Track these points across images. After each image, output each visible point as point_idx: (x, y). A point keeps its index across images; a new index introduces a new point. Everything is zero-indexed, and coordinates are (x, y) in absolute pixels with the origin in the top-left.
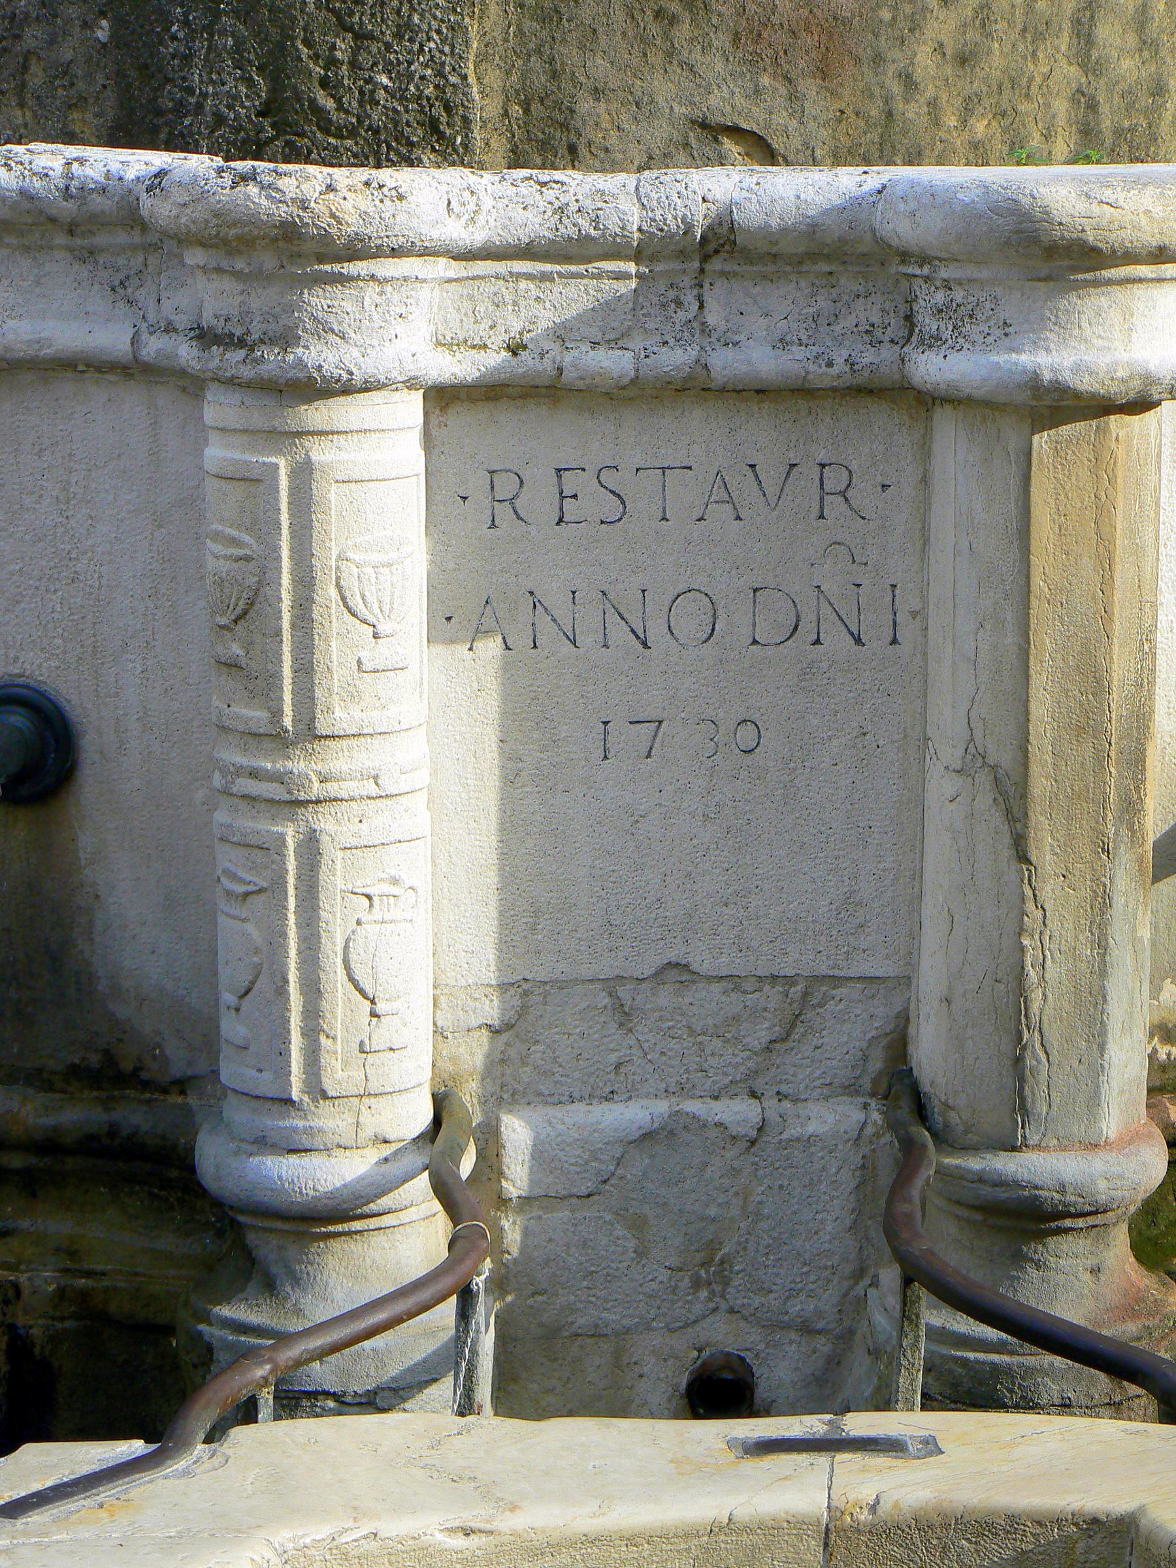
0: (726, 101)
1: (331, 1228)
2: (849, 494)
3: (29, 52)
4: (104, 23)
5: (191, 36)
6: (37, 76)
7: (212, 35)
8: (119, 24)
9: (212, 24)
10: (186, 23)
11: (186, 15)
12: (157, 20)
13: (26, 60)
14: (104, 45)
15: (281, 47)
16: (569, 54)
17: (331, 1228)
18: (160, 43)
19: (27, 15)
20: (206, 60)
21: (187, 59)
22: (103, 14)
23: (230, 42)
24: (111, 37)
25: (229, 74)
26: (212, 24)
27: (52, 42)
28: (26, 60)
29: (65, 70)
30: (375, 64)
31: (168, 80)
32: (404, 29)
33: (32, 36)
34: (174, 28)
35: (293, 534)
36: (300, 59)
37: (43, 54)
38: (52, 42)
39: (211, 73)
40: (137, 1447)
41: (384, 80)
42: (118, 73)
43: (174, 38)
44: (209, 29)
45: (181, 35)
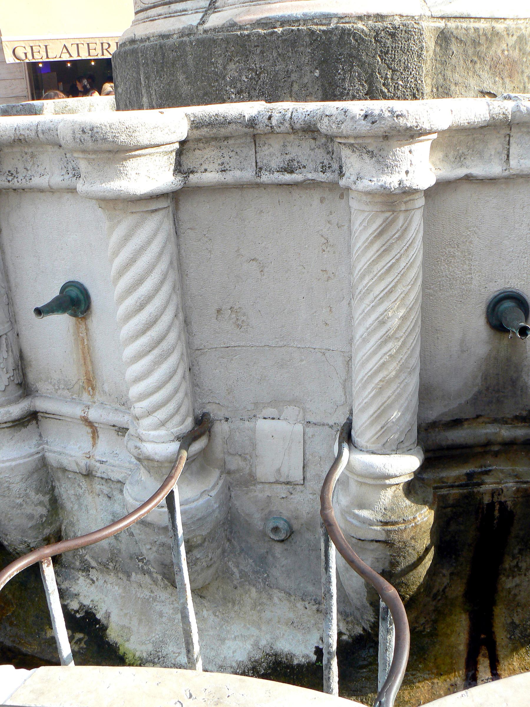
0: (488, 86)
4: (317, 71)
5: (345, 73)
6: (296, 87)
7: (351, 73)
8: (322, 71)
10: (343, 69)
11: (343, 67)
13: (292, 83)
15: (372, 74)
16: (449, 73)
19: (292, 70)
21: (344, 80)
22: (317, 68)
23: (357, 74)
27: (301, 77)
28: (292, 83)
32: (406, 68)
33: (294, 77)
34: (339, 71)
37: (298, 81)
38: (301, 77)
41: (401, 83)
43: (339, 74)
45: (342, 73)
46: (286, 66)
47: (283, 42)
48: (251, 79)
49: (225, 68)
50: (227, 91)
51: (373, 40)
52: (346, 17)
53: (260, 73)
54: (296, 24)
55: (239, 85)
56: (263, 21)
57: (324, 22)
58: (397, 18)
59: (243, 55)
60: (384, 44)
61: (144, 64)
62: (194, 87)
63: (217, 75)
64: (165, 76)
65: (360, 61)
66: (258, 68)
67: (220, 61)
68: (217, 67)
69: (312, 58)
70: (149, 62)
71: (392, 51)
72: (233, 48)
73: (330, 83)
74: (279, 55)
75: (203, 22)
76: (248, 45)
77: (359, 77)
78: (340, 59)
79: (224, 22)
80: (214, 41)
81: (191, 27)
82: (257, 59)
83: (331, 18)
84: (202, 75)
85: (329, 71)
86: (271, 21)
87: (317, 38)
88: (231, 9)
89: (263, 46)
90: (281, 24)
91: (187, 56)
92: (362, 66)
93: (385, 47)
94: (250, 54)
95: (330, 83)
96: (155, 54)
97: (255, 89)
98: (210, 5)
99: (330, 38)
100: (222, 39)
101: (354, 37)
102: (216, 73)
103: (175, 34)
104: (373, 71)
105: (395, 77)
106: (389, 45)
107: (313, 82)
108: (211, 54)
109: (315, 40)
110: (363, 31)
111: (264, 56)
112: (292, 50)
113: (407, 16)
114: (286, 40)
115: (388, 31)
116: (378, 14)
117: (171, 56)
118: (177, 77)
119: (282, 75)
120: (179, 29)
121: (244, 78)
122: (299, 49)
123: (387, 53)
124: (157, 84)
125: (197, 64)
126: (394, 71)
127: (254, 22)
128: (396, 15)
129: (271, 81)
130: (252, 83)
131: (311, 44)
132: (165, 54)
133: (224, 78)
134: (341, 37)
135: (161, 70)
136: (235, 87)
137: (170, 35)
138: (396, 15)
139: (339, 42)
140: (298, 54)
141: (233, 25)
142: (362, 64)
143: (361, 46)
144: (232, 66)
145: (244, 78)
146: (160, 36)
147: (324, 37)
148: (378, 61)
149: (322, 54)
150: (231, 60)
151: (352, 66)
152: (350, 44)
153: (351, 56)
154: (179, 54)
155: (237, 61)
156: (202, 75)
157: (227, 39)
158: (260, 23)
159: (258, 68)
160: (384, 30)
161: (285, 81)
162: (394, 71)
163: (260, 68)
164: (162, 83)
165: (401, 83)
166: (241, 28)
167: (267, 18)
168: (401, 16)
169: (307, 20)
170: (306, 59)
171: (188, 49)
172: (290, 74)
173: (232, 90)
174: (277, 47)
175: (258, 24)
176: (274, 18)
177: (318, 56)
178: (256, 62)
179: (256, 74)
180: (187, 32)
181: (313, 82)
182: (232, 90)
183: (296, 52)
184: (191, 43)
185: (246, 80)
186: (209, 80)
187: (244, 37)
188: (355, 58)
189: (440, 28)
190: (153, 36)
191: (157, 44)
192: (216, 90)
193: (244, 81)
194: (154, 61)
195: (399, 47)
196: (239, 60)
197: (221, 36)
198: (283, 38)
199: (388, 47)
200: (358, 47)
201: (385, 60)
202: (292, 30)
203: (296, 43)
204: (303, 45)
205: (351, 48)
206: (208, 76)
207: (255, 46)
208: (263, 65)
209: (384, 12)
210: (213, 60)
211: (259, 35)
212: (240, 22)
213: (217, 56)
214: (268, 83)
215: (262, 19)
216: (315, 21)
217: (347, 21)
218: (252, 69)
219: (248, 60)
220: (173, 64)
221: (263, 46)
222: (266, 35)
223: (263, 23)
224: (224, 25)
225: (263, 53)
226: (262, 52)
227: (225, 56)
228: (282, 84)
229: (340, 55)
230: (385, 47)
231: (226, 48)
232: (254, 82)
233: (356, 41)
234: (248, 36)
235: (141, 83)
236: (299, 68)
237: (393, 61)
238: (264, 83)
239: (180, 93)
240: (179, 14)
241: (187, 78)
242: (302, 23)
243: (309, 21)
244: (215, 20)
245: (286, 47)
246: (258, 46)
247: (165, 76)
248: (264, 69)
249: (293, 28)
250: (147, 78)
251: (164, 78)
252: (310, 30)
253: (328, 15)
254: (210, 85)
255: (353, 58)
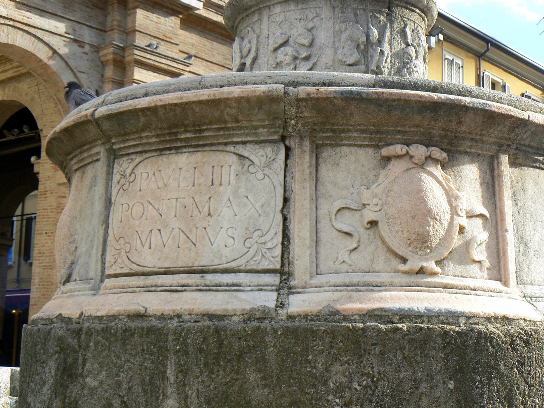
1: (415, 9)
2: (131, 184)
3: (422, 393)
4: (452, 382)
5: (483, 387)
7: (489, 386)
8: (457, 382)
9: (489, 382)
10: (481, 382)
11: (481, 378)
12: (470, 381)
13: (420, 396)
14: (452, 390)
15: (511, 390)
17: (415, 9)
18: (472, 390)
19: (421, 379)
20: (488, 395)
21: (482, 395)
22: (451, 379)
23: (496, 389)
24: (454, 387)
25: (496, 400)
26: (489, 382)
27: (432, 389)
28: (420, 396)
29: (437, 400)
30: (535, 396)
31: (475, 403)
33: (423, 388)
34: (477, 384)
35: (401, 88)
36: (517, 394)
37: (428, 394)
38: (432, 389)
39: (490, 400)
40: (21, 206)
41: (537, 401)
42: (457, 401)
43: (477, 387)
44: (488, 384)
45: (480, 386)
46: (414, 373)
47: (410, 342)
48: (365, 387)
49: (327, 370)
50: (328, 401)
51: (510, 347)
52: (474, 316)
53: (378, 380)
54: (419, 321)
55: (347, 395)
56: (376, 313)
57: (451, 320)
58: (522, 322)
59: (355, 354)
60: (521, 353)
61: (178, 351)
62: (275, 391)
63: (315, 378)
64: (221, 373)
65: (498, 372)
66: (376, 374)
67: (321, 360)
68: (315, 367)
69: (445, 365)
70: (191, 349)
71: (528, 362)
72: (341, 344)
73: (466, 398)
74: (405, 358)
75: (281, 305)
76: (364, 342)
77: (498, 392)
78: (477, 369)
79: (320, 308)
80: (313, 332)
81: (267, 310)
82: (375, 361)
83: (459, 316)
84: (291, 377)
85: (465, 383)
86: (387, 313)
87: (451, 340)
88: (318, 292)
89: (384, 345)
90: (400, 319)
91: (266, 348)
92: (500, 378)
93: (522, 357)
94: (365, 354)
95: (466, 398)
96: (205, 339)
97: (370, 401)
98: (281, 282)
99: (465, 341)
100: (325, 331)
101: (491, 343)
102: (314, 376)
103: (235, 315)
104: (512, 386)
105: (532, 394)
106: (524, 355)
107: (447, 395)
108: (307, 349)
109: (448, 343)
110: (499, 336)
111: (384, 358)
112: (421, 353)
113: (530, 321)
114: (413, 339)
115: (522, 338)
116: (504, 316)
117: (237, 345)
118: (244, 376)
119: (407, 385)
120: (244, 310)
121: (356, 385)
122: (430, 352)
123: (523, 364)
124: (203, 382)
125: (283, 361)
126: (530, 386)
127: (364, 313)
128: (521, 319)
129: (394, 391)
130: (367, 392)
131: (444, 347)
132: (223, 341)
133: (325, 383)
134: (478, 342)
135: (214, 363)
136: (341, 397)
137: (225, 316)
138: (521, 319)
139: (475, 348)
140: (428, 359)
141: (333, 314)
142: (500, 377)
143: (498, 354)
144: (337, 368)
145: (356, 385)
146: (204, 315)
147: (459, 340)
148: (516, 374)
149: (457, 361)
150: (336, 360)
151: (490, 378)
152: (488, 350)
153: (488, 365)
154: (251, 344)
155: (346, 362)
156: (291, 377)
157: (333, 332)
158: (372, 315)
159: (376, 374)
160: (518, 336)
161: (411, 392)
162: (530, 386)
163: (379, 373)
164: (213, 380)
165: (537, 401)
166: (345, 318)
167: (381, 309)
168: (525, 320)
169: (432, 316)
170: (438, 366)
171: (269, 339)
172: (418, 384)
173: (337, 400)
174: (402, 349)
175: (370, 316)
176: (390, 310)
177: (452, 363)
178: (373, 365)
179: (373, 381)
180: (258, 315)
181: (447, 395)
182: (337, 400)
183: (426, 356)
184: (275, 331)
185: (358, 388)
186: (301, 383)
187: (357, 331)
188: (493, 368)
189: (245, 309)
190: (190, 314)
191: (209, 327)
192: (312, 398)
193: (355, 389)
194: (201, 350)
195: (533, 357)
196: (349, 360)
197: (323, 326)
198: (410, 336)
199: (525, 357)
200: (496, 355)
201: (522, 372)
202: (421, 329)
203: (426, 344)
204: (435, 348)
205: (488, 355)
206: (301, 378)
207: (373, 345)
208: (383, 370)
209: (510, 315)
210: (310, 357)
211: (378, 331)
212: (344, 310)
213: (316, 352)
214: (389, 393)
215: (375, 310)
216: (441, 318)
217: (475, 322)
218: (368, 375)
219: (362, 362)
220: (240, 357)
221: (384, 345)
222: (388, 331)
223: (376, 315)
224: (320, 311)
225: (383, 354)
226: (382, 353)
227: (329, 353)
228: (407, 397)
229: (477, 363)
230: (522, 357)
231: (331, 342)
232: (370, 392)
233: (493, 347)
234: (363, 330)
235: (164, 377)
236: (430, 376)
237: (529, 374)
238: (383, 393)
239: (248, 399)
240: (228, 288)
241: (263, 379)
242: (425, 319)
243: (434, 318)
244: (298, 304)
245: (413, 349)
246: (376, 344)
247: (221, 373)
248: (384, 376)
249: (422, 325)
250: (183, 371)
251: (218, 375)
252: (443, 329)
253: (455, 313)
254: (302, 391)
255: (490, 368)
